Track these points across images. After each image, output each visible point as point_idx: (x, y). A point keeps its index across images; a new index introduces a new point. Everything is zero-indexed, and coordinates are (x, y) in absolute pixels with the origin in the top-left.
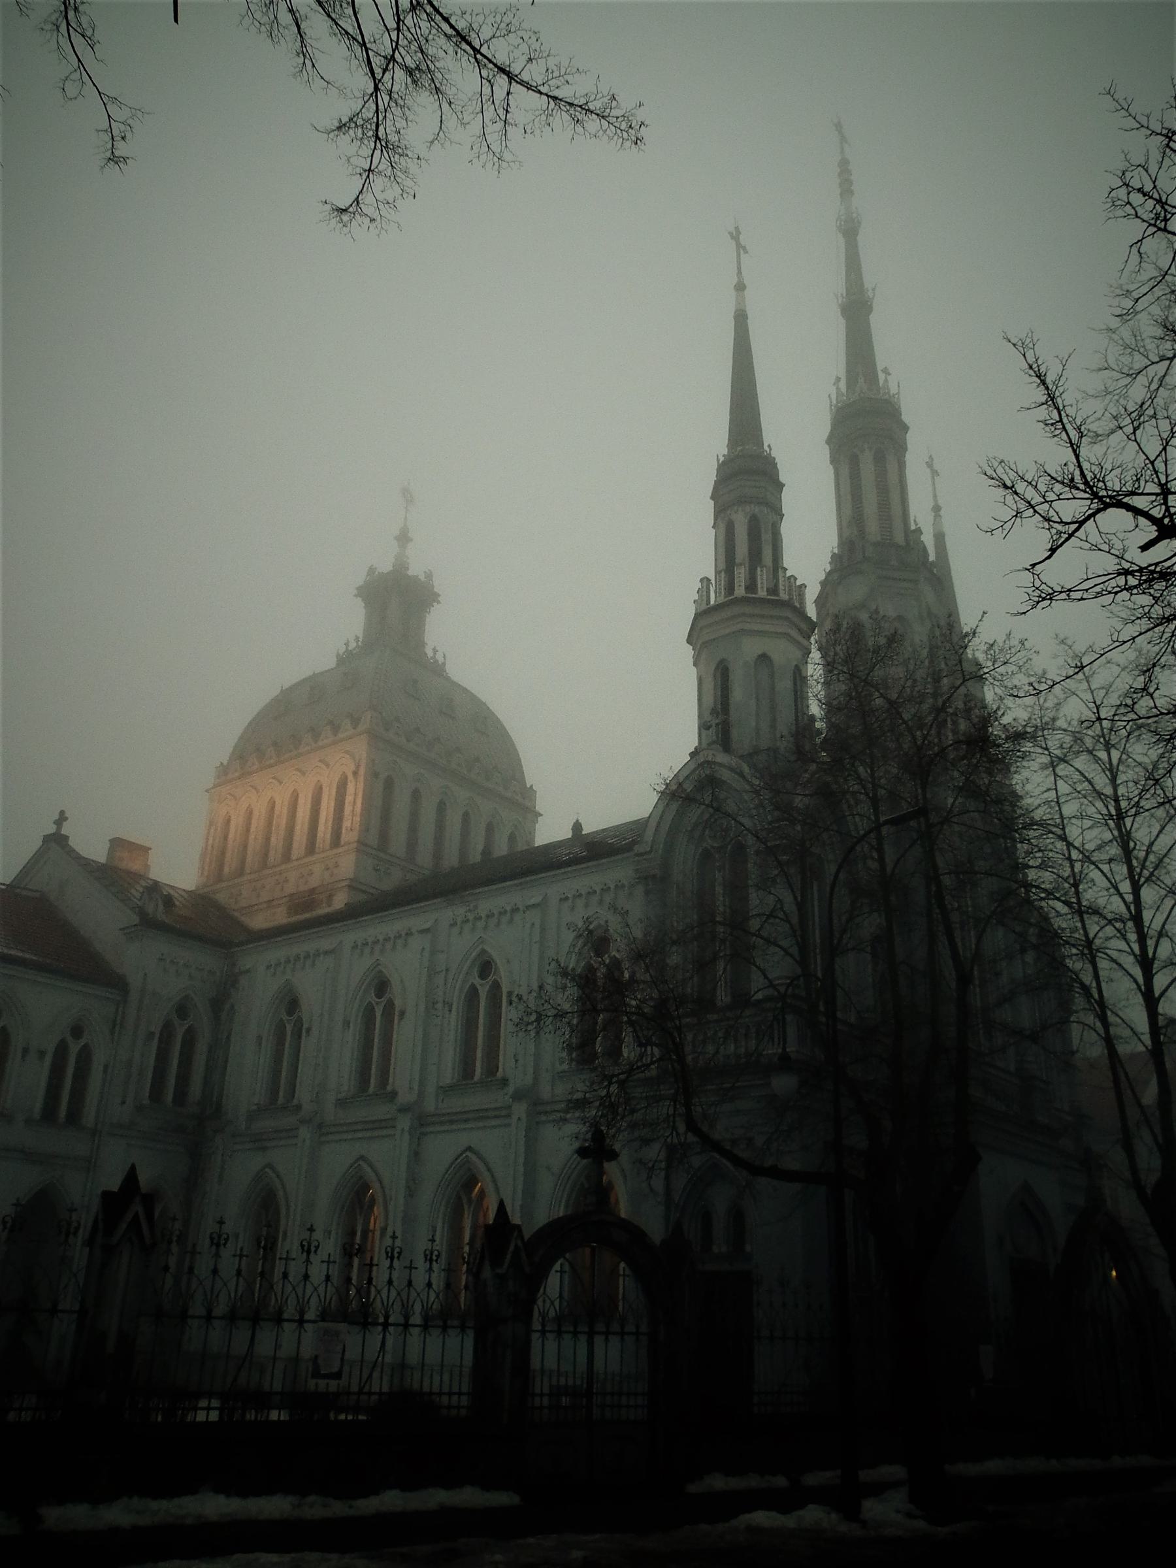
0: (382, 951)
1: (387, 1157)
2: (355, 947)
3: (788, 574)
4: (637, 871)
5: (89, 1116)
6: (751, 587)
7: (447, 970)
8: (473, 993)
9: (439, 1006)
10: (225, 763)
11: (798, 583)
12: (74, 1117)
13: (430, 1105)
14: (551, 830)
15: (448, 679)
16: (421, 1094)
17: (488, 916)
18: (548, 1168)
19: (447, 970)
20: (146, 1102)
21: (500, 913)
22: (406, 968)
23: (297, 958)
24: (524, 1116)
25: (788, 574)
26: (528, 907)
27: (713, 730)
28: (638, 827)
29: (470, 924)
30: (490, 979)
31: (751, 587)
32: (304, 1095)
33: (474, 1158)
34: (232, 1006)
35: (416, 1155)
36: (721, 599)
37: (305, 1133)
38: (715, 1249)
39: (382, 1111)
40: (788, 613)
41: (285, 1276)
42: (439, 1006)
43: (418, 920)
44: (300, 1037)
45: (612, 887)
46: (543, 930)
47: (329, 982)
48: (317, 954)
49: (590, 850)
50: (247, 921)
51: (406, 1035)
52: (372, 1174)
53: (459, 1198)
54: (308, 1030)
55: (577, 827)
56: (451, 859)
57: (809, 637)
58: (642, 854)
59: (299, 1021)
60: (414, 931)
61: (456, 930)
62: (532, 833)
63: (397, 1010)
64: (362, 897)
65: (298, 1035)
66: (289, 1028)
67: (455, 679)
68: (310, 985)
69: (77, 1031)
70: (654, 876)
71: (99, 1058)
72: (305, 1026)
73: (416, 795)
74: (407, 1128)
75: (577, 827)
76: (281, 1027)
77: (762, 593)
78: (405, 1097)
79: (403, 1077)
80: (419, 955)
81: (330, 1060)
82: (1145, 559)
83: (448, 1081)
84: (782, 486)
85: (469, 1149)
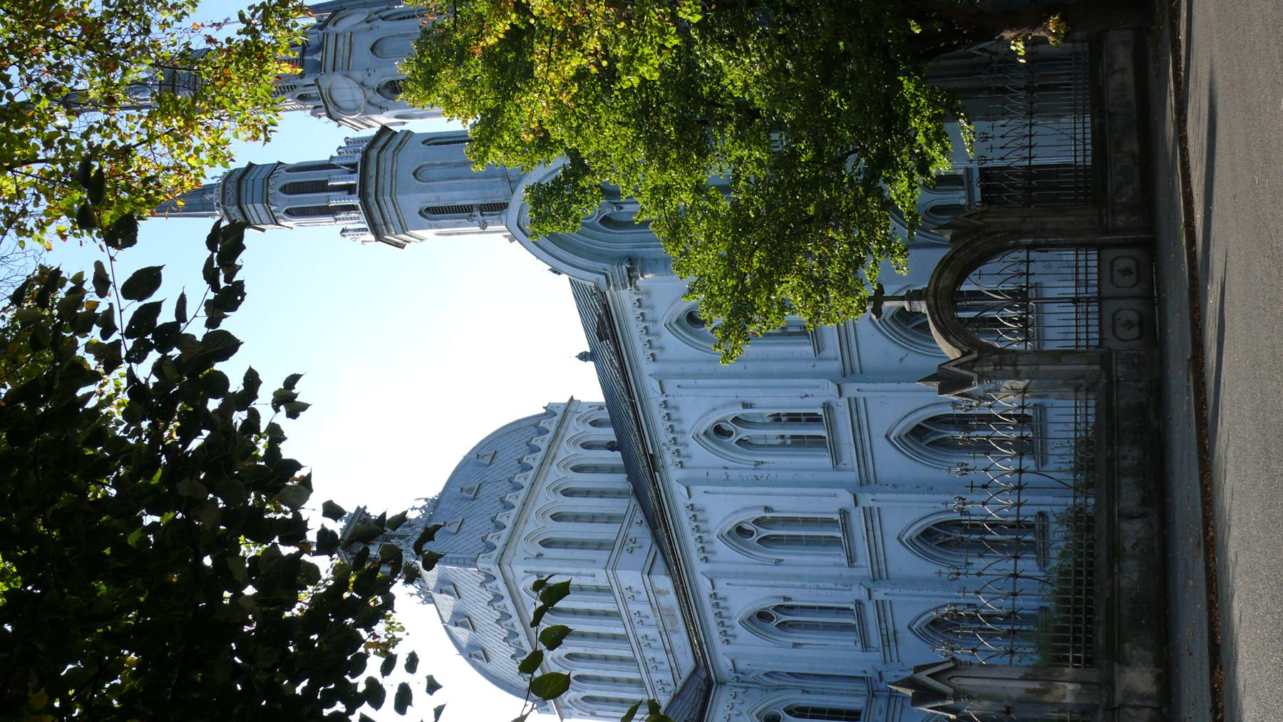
1: (903, 515)
2: (706, 560)
3: (336, 154)
4: (624, 287)
6: (349, 189)
7: (726, 468)
9: (759, 473)
11: (344, 145)
13: (853, 476)
14: (587, 387)
15: (442, 494)
16: (840, 485)
18: (901, 360)
19: (726, 468)
22: (724, 508)
23: (719, 615)
24: (857, 386)
25: (336, 154)
26: (663, 392)
27: (488, 219)
28: (579, 292)
29: (701, 524)
30: (773, 613)
31: (349, 189)
32: (846, 598)
33: (906, 536)
34: (766, 674)
35: (896, 487)
36: (363, 218)
37: (879, 595)
38: (963, 202)
39: (857, 522)
40: (374, 153)
41: (1002, 159)
42: (759, 473)
45: (644, 324)
46: (682, 376)
48: (714, 596)
49: (605, 332)
50: (686, 673)
51: (787, 503)
54: (786, 599)
55: (583, 357)
56: (619, 481)
57: (395, 133)
58: (608, 281)
60: (689, 503)
61: (686, 462)
62: (591, 405)
65: (773, 522)
66: (766, 533)
67: (440, 490)
70: (629, 270)
72: (761, 514)
73: (557, 517)
74: (872, 497)
75: (583, 357)
77: (354, 180)
80: (710, 498)
81: (810, 576)
84: (251, 165)
85: (887, 437)
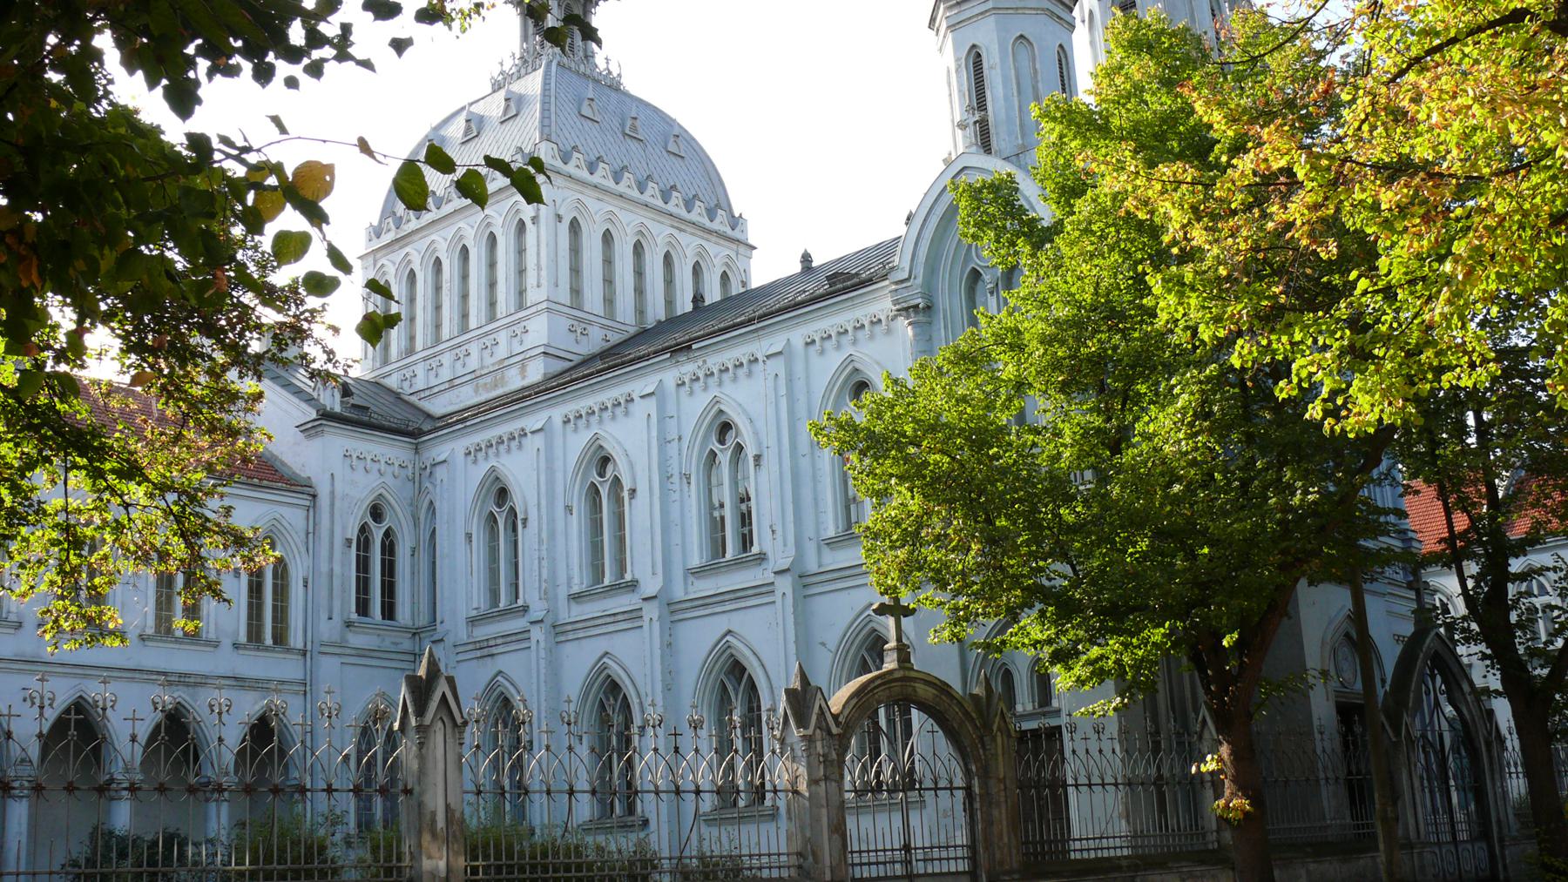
0: (601, 421)
5: (296, 639)
8: (594, 491)
9: (676, 479)
10: (375, 223)
12: (280, 638)
13: (679, 593)
14: (769, 265)
17: (750, 362)
20: (354, 616)
21: (839, 334)
26: (768, 357)
27: (970, 131)
29: (687, 388)
32: (530, 594)
35: (669, 646)
37: (537, 634)
42: (676, 479)
43: (641, 384)
44: (515, 529)
45: (867, 324)
46: (790, 380)
47: (538, 463)
51: (641, 516)
52: (748, 653)
53: (602, 706)
54: (525, 521)
55: (806, 259)
56: (656, 311)
58: (902, 281)
59: (513, 511)
60: (635, 396)
63: (626, 488)
64: (560, 366)
65: (617, 500)
68: (520, 470)
69: (376, 513)
70: (917, 306)
71: (297, 574)
72: (520, 516)
73: (607, 238)
74: (655, 618)
75: (806, 259)
76: (594, 491)
78: (651, 586)
79: (644, 566)
81: (554, 549)
82: (266, 386)
83: (831, 533)
